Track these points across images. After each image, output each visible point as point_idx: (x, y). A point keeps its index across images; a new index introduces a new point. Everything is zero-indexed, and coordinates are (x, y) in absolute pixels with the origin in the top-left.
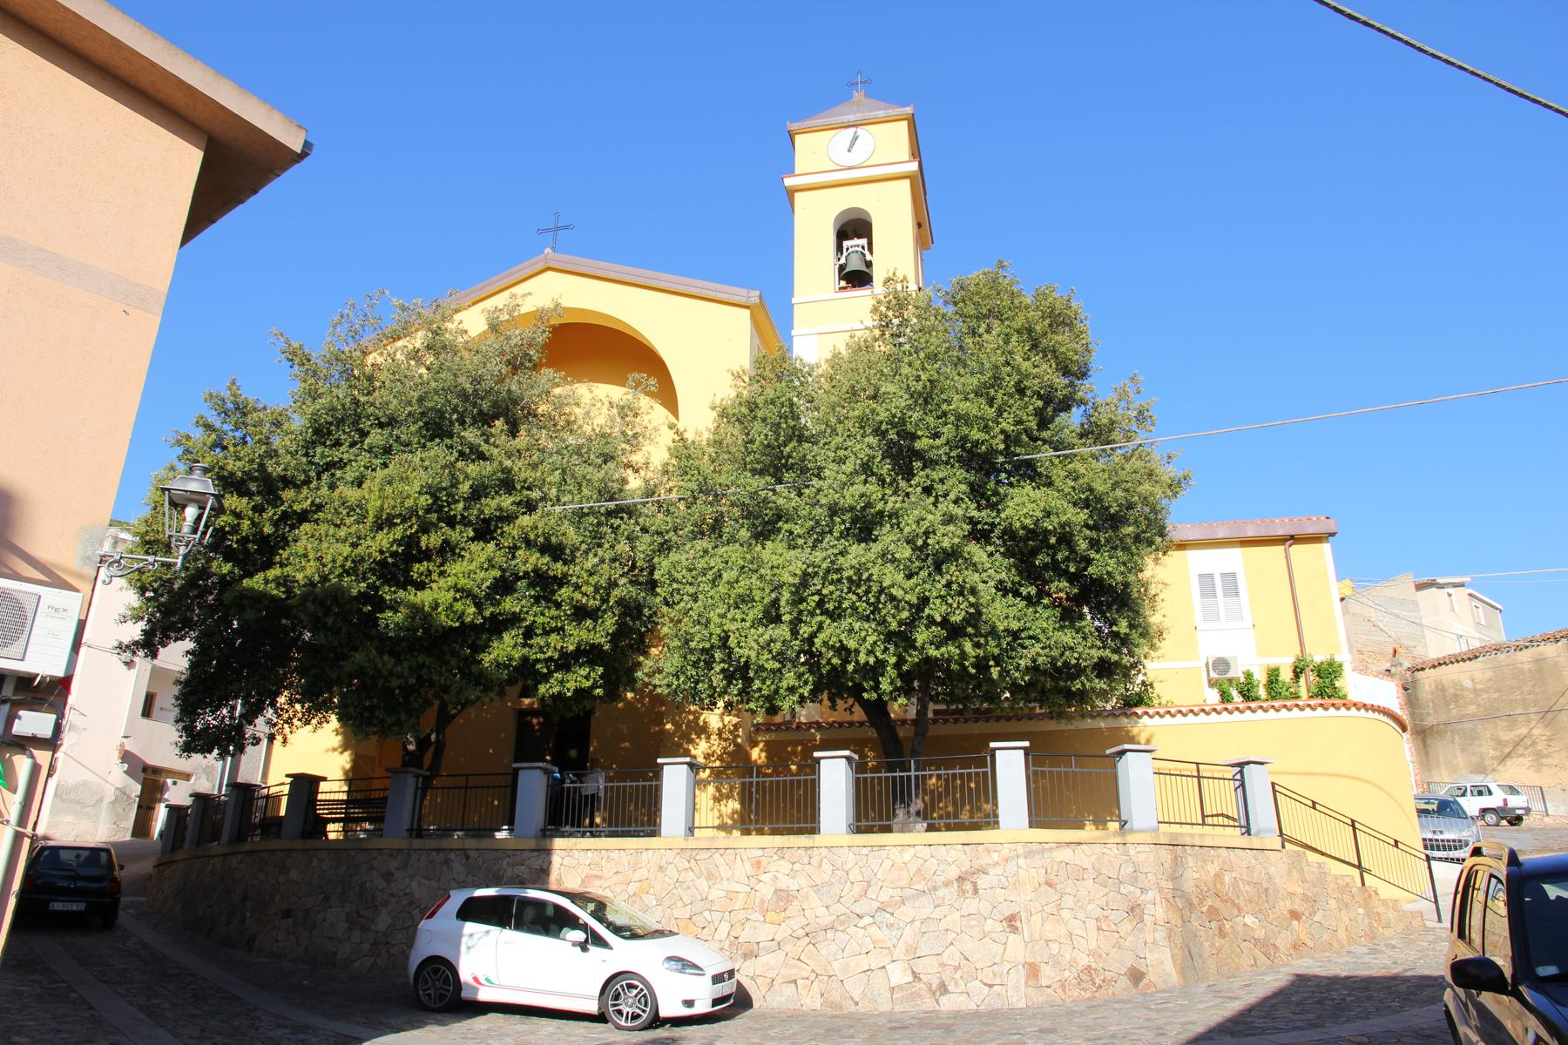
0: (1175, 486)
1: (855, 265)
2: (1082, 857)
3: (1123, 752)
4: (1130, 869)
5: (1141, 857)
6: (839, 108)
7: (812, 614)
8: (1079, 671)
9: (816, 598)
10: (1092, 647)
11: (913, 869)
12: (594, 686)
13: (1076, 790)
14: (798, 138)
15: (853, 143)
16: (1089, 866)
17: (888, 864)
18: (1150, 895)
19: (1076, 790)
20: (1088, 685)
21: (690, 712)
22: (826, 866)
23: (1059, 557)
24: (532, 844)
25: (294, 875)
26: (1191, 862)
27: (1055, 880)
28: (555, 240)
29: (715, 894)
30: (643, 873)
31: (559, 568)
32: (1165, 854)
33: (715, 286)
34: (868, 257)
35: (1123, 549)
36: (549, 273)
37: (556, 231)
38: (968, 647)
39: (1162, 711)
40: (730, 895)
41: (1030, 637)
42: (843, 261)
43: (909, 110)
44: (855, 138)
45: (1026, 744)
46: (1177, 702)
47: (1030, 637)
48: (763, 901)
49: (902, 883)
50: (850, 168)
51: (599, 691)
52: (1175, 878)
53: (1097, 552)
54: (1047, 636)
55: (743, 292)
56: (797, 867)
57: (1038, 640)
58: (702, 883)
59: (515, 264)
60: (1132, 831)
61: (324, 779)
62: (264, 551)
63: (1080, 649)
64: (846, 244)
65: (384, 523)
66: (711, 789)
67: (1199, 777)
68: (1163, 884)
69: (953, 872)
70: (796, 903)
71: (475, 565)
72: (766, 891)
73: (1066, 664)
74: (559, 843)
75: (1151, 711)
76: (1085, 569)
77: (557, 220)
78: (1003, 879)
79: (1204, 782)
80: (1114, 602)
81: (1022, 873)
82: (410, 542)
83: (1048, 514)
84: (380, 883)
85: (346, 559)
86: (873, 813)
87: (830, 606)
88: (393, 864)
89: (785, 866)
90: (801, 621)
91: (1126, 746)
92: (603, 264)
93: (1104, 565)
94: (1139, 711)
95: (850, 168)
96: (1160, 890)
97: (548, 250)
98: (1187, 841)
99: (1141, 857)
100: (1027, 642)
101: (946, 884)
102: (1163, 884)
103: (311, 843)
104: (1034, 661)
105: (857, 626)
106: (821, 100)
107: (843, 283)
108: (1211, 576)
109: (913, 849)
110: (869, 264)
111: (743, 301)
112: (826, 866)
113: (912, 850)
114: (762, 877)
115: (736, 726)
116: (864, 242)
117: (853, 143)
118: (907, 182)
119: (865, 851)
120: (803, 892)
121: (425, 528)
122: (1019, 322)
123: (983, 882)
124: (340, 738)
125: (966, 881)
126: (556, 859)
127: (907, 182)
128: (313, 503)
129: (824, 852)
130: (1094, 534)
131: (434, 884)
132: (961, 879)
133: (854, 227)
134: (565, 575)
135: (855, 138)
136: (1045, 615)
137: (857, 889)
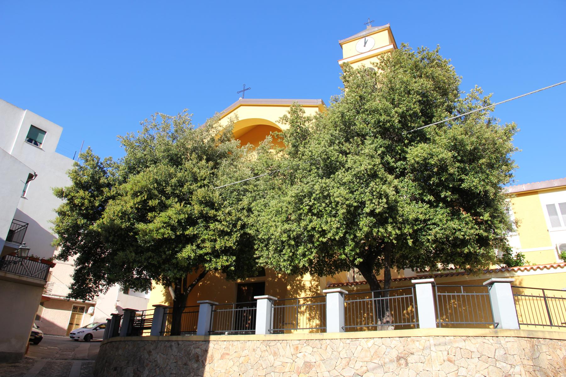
0: (508, 133)
2: (471, 345)
3: (492, 283)
4: (502, 352)
5: (509, 345)
7: (306, 215)
8: (464, 243)
9: (307, 207)
10: (472, 228)
11: (373, 351)
12: (230, 265)
13: (464, 306)
14: (343, 46)
15: (365, 43)
16: (475, 350)
17: (359, 348)
18: (518, 369)
19: (464, 306)
20: (472, 250)
21: (298, 280)
22: (329, 349)
23: (443, 179)
24: (202, 338)
25: (120, 352)
26: (544, 349)
27: (453, 358)
28: (243, 95)
29: (277, 363)
30: (246, 352)
31: (212, 212)
32: (525, 343)
35: (482, 173)
36: (241, 107)
37: (244, 91)
38: (390, 228)
39: (528, 268)
40: (284, 364)
41: (434, 224)
43: (388, 25)
45: (432, 280)
46: (537, 264)
47: (434, 224)
48: (298, 368)
49: (367, 359)
51: (233, 268)
52: (534, 358)
53: (466, 175)
54: (443, 223)
56: (315, 350)
57: (438, 226)
58: (271, 358)
59: (227, 104)
60: (503, 330)
61: (138, 311)
62: (95, 213)
63: (464, 230)
65: (135, 195)
66: (307, 315)
67: (545, 297)
68: (525, 362)
69: (394, 354)
70: (314, 369)
71: (174, 212)
72: (300, 363)
73: (456, 238)
74: (213, 338)
75: (522, 268)
76: (400, 128)
77: (244, 87)
78: (422, 358)
79: (549, 302)
80: (480, 204)
81: (433, 354)
82: (144, 202)
83: (432, 156)
84: (147, 356)
85: (119, 212)
86: (353, 321)
87: (315, 211)
88: (152, 347)
89: (309, 349)
90: (301, 219)
91: (494, 279)
93: (471, 182)
94: (516, 269)
96: (524, 366)
97: (241, 98)
98: (540, 335)
99: (509, 345)
100: (431, 227)
101: (391, 361)
102: (525, 362)
103: (134, 338)
104: (435, 236)
105: (329, 219)
108: (554, 205)
109: (383, 340)
112: (329, 349)
113: (372, 341)
114: (299, 355)
115: (317, 286)
117: (365, 43)
119: (348, 341)
120: (317, 363)
121: (151, 196)
123: (410, 359)
124: (165, 297)
125: (402, 359)
126: (211, 345)
128: (116, 193)
129: (328, 342)
130: (462, 165)
131: (165, 356)
132: (399, 359)
134: (215, 216)
136: (441, 212)
137: (344, 362)
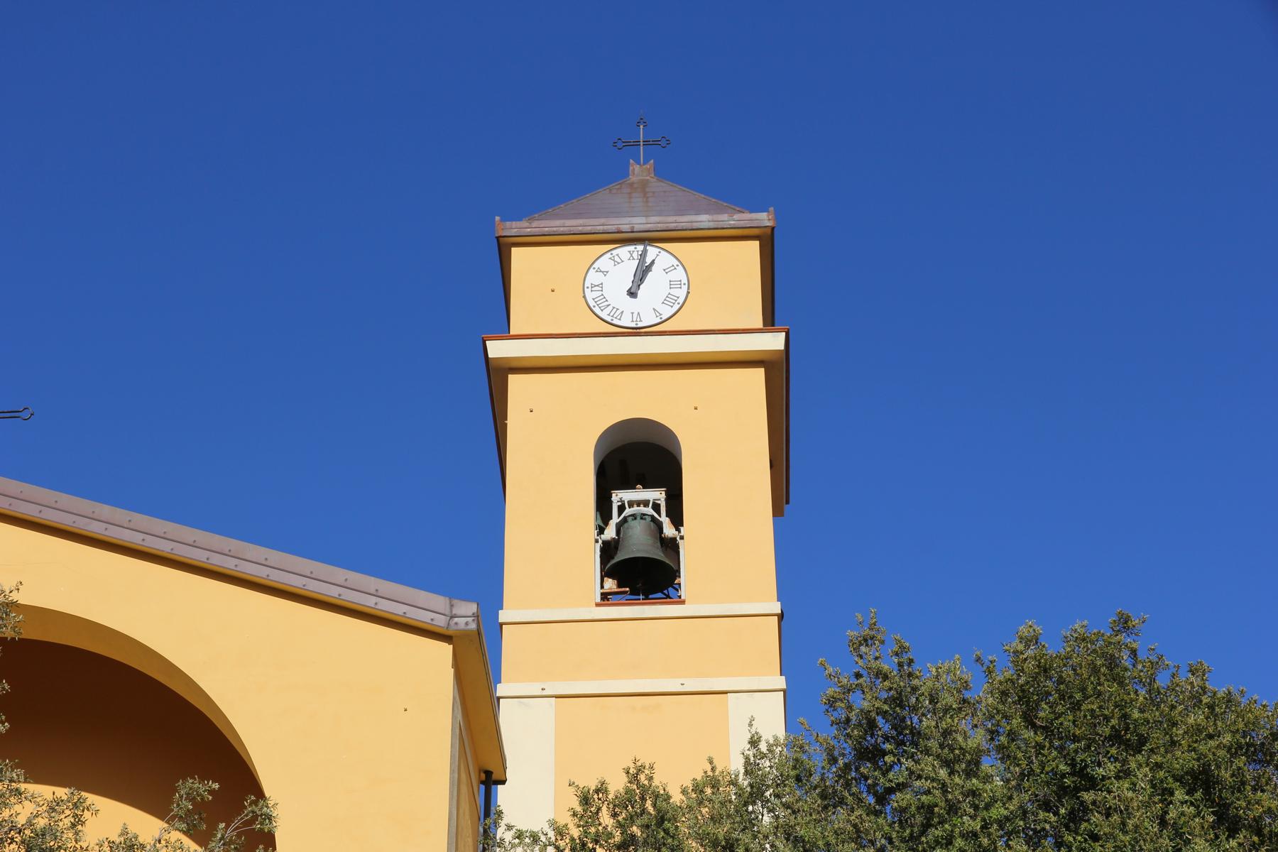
1: (639, 544)
6: (601, 197)
33: (372, 583)
34: (669, 531)
42: (610, 533)
43: (764, 219)
44: (643, 272)
50: (636, 332)
55: (440, 602)
64: (619, 496)
92: (106, 510)
95: (636, 332)
106: (569, 180)
107: (610, 584)
110: (671, 546)
111: (440, 622)
116: (658, 495)
118: (760, 373)
122: (1183, 760)
127: (760, 373)
133: (638, 458)
135: (643, 272)
